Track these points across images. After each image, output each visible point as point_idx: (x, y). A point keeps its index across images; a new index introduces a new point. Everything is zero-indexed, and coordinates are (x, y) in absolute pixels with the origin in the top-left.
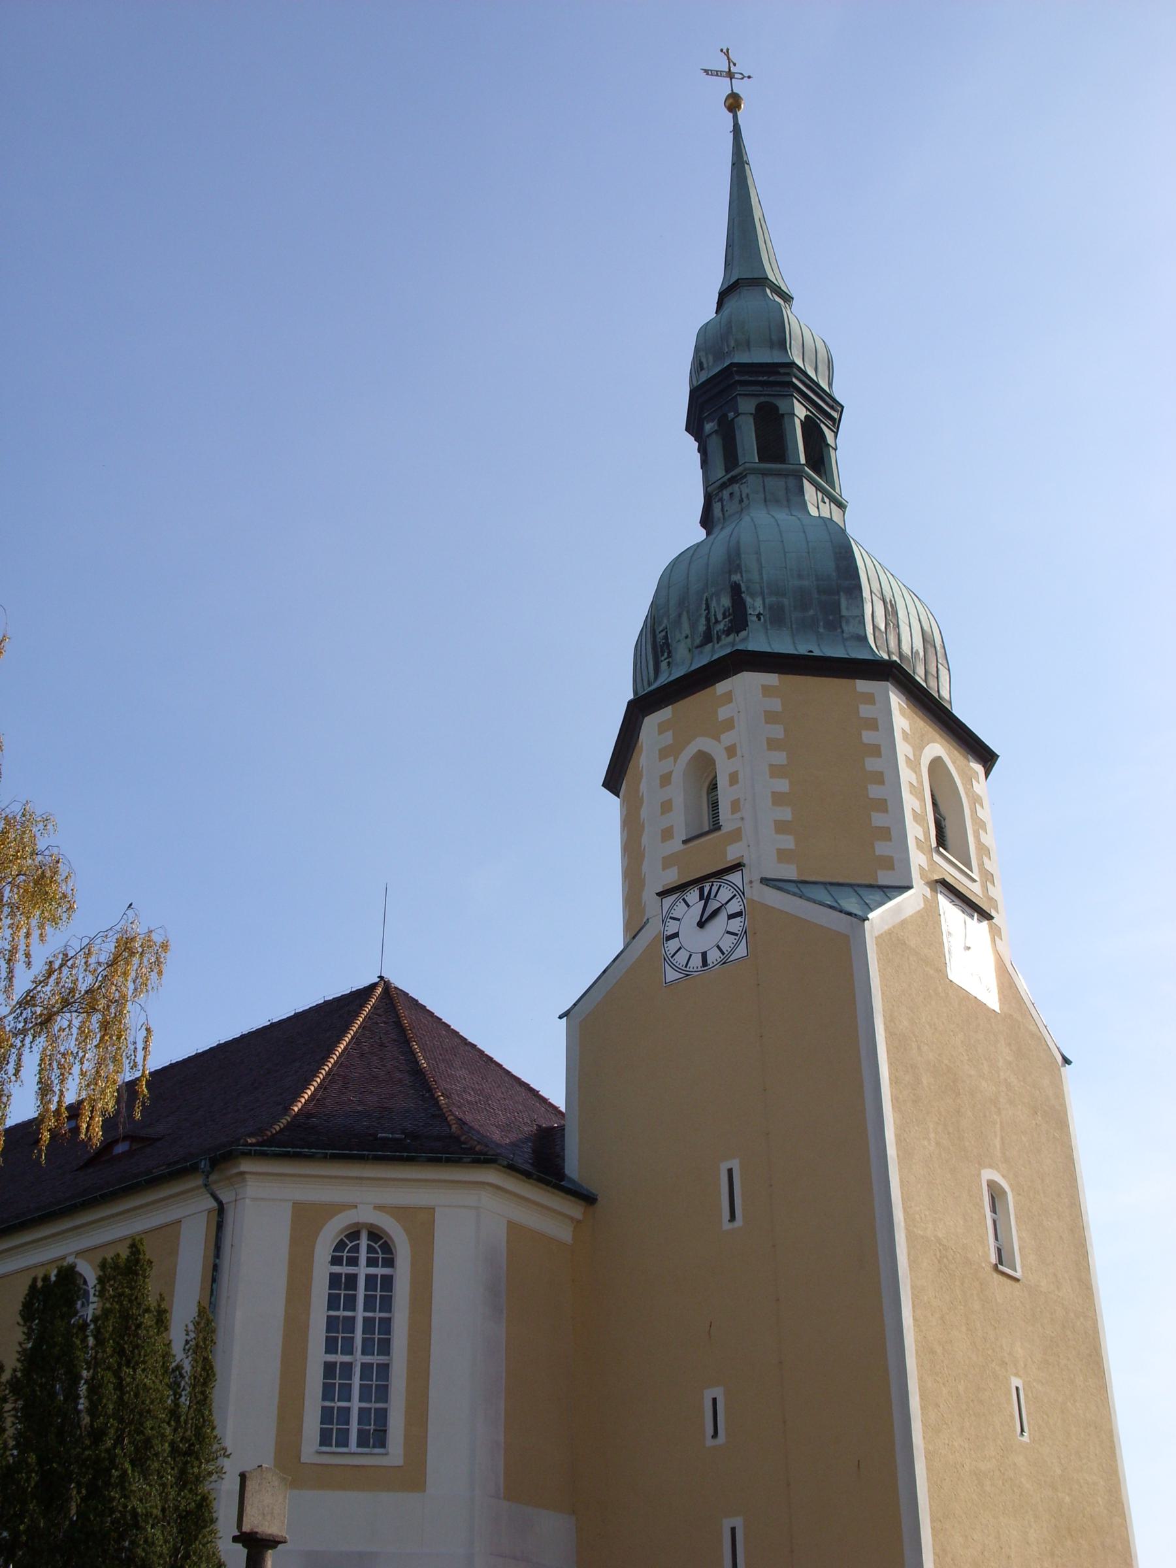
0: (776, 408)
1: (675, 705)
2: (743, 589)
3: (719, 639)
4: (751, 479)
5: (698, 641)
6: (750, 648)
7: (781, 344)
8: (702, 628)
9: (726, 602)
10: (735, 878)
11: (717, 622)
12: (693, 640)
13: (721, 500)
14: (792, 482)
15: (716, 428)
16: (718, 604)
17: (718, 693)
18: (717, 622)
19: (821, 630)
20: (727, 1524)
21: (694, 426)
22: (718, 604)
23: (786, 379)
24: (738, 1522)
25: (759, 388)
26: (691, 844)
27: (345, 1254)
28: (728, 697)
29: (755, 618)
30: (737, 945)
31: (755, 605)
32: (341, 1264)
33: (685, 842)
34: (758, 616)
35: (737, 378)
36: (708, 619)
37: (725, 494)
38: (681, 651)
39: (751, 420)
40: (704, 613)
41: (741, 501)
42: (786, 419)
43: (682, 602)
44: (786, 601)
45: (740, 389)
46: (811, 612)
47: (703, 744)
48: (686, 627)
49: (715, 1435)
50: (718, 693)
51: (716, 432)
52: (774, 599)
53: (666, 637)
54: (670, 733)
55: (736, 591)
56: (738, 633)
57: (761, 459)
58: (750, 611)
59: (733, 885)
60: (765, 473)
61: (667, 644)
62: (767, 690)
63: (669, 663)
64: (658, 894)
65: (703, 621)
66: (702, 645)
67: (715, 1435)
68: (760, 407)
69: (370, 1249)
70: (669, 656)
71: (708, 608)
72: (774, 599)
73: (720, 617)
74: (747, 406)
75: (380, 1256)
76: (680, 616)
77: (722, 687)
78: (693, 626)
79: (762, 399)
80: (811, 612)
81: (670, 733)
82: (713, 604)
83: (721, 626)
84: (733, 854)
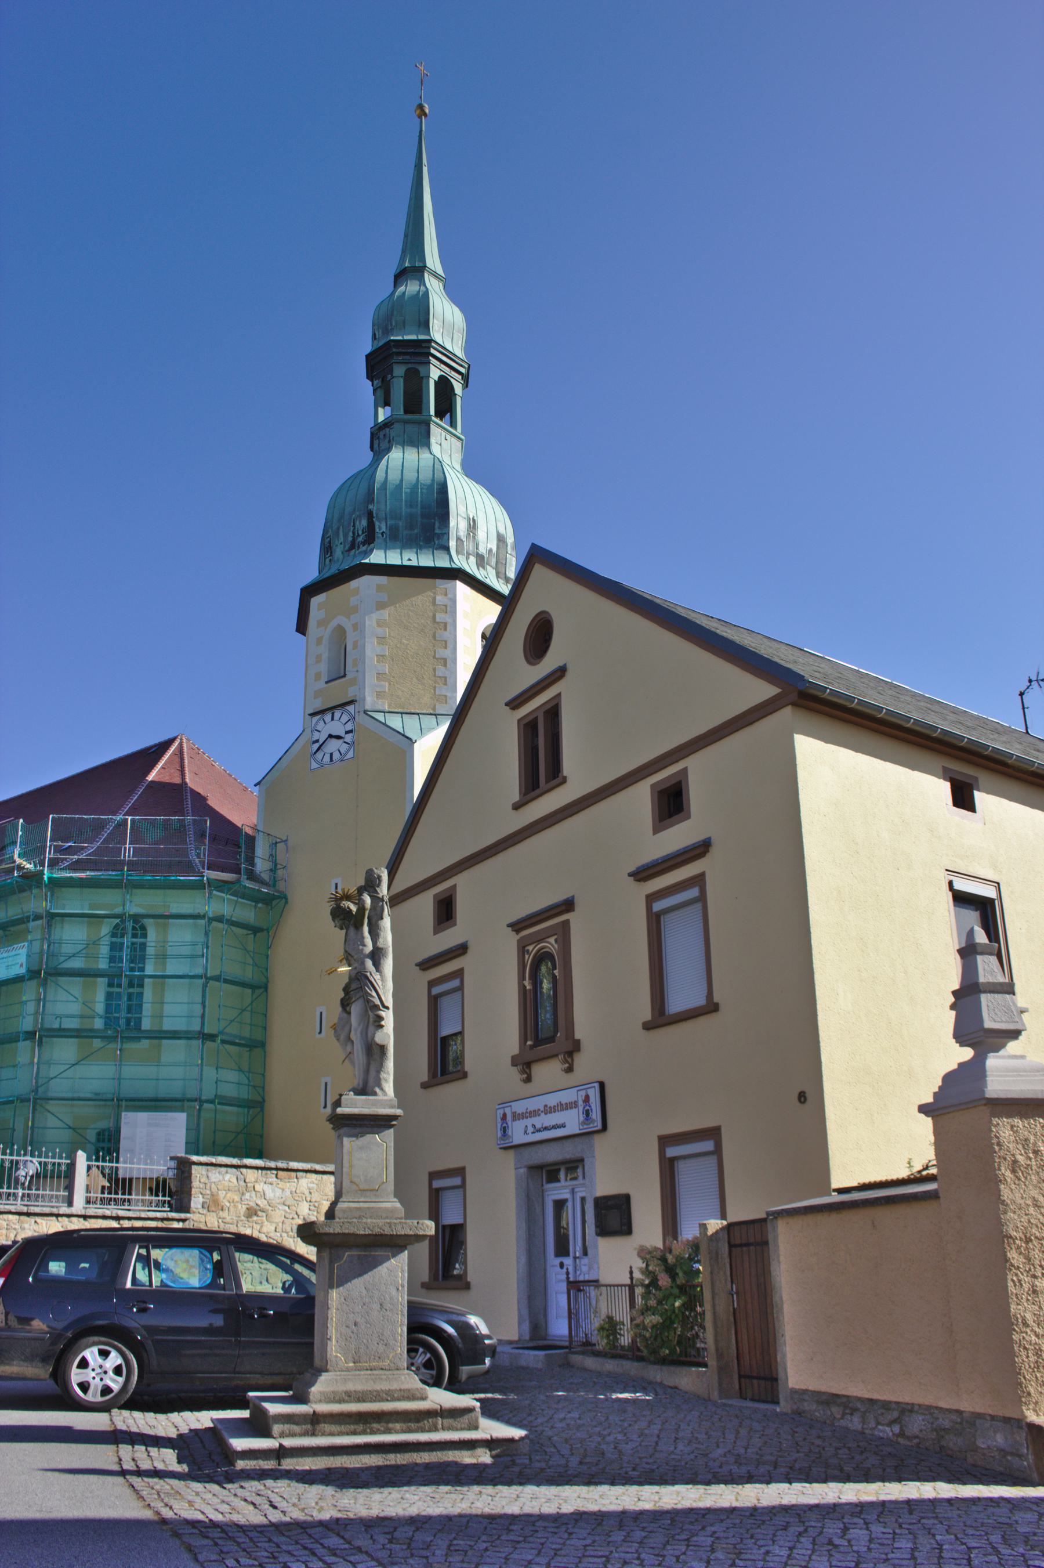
0: (418, 372)
1: (330, 592)
2: (375, 515)
3: (359, 547)
4: (396, 426)
5: (347, 548)
6: (372, 561)
7: (424, 324)
8: (350, 539)
9: (364, 523)
10: (351, 708)
11: (359, 535)
12: (344, 547)
13: (378, 438)
14: (423, 427)
15: (380, 385)
16: (360, 523)
17: (352, 588)
18: (359, 535)
19: (421, 543)
20: (323, 1080)
21: (370, 376)
22: (360, 523)
23: (426, 351)
24: (328, 1080)
25: (408, 357)
26: (330, 684)
27: (119, 931)
28: (357, 591)
29: (380, 535)
30: (349, 750)
31: (381, 527)
32: (117, 937)
33: (327, 683)
34: (382, 534)
35: (394, 350)
36: (354, 533)
37: (381, 434)
38: (338, 552)
39: (402, 380)
40: (352, 528)
41: (389, 441)
42: (424, 381)
43: (341, 517)
44: (401, 523)
45: (395, 359)
46: (416, 531)
47: (340, 620)
48: (342, 539)
49: (320, 1032)
50: (352, 588)
51: (380, 387)
52: (393, 522)
53: (330, 542)
54: (323, 611)
55: (370, 515)
56: (369, 544)
57: (406, 412)
58: (377, 530)
59: (350, 714)
60: (406, 422)
61: (330, 547)
62: (380, 588)
63: (330, 560)
64: (310, 715)
65: (351, 534)
66: (350, 550)
67: (320, 1032)
68: (407, 371)
69: (134, 928)
70: (331, 556)
71: (354, 526)
72: (393, 522)
73: (360, 533)
74: (399, 371)
75: (139, 932)
76: (338, 529)
77: (354, 584)
78: (345, 536)
79: (410, 366)
80: (416, 531)
81: (323, 611)
82: (357, 523)
83: (360, 539)
84: (351, 693)
